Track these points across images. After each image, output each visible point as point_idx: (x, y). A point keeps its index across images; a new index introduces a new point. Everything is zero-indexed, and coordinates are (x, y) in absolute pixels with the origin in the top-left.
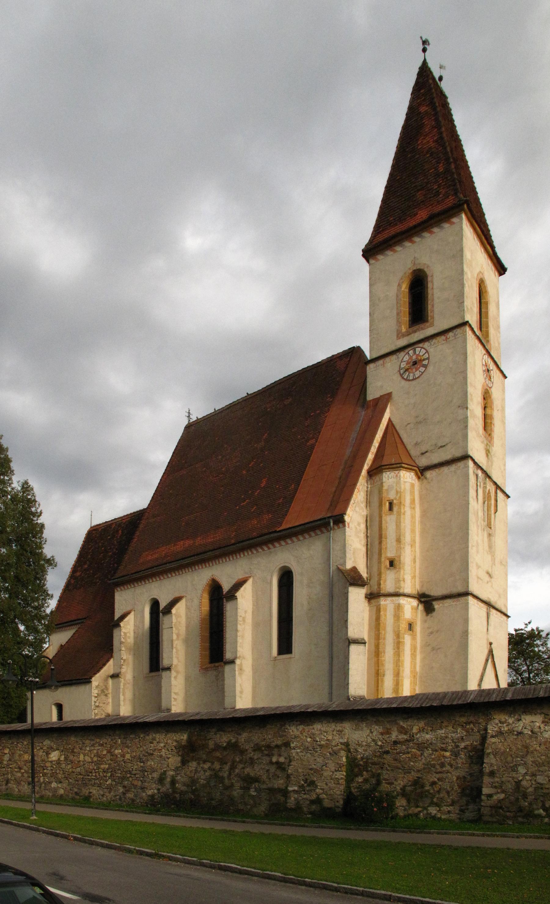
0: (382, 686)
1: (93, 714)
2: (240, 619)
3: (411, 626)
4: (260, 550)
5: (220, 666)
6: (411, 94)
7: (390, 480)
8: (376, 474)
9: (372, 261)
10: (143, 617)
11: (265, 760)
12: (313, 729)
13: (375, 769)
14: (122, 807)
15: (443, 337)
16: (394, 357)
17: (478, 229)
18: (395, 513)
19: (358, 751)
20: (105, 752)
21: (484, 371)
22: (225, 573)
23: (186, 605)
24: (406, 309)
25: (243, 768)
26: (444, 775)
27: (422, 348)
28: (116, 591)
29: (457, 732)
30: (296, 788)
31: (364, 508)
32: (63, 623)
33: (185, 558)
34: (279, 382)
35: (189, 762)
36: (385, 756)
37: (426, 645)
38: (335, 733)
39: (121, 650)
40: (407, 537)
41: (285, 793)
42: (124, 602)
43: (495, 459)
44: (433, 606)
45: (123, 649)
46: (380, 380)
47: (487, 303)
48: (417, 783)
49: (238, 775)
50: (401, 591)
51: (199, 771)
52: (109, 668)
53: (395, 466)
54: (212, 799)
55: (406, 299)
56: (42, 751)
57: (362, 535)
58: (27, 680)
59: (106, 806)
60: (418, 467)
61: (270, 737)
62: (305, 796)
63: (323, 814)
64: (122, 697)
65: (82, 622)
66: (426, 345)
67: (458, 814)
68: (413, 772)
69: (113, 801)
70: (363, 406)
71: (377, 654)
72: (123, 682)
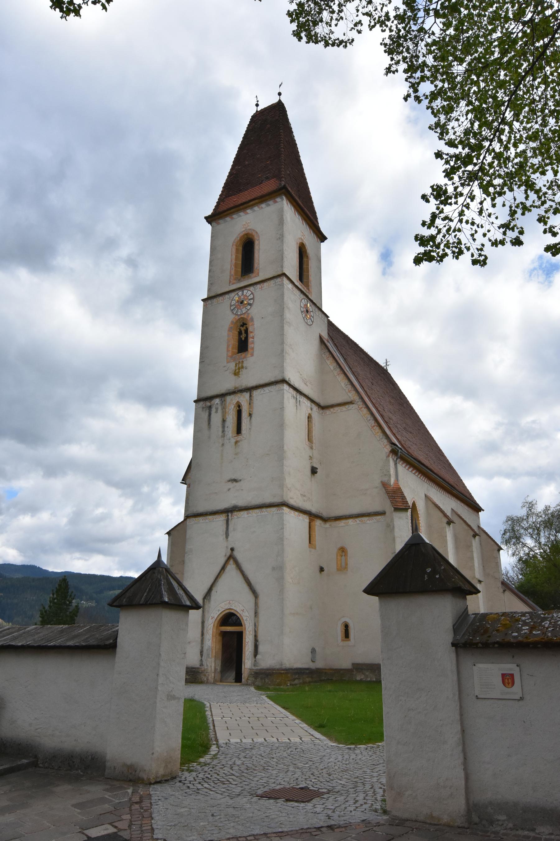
66: (252, 288)
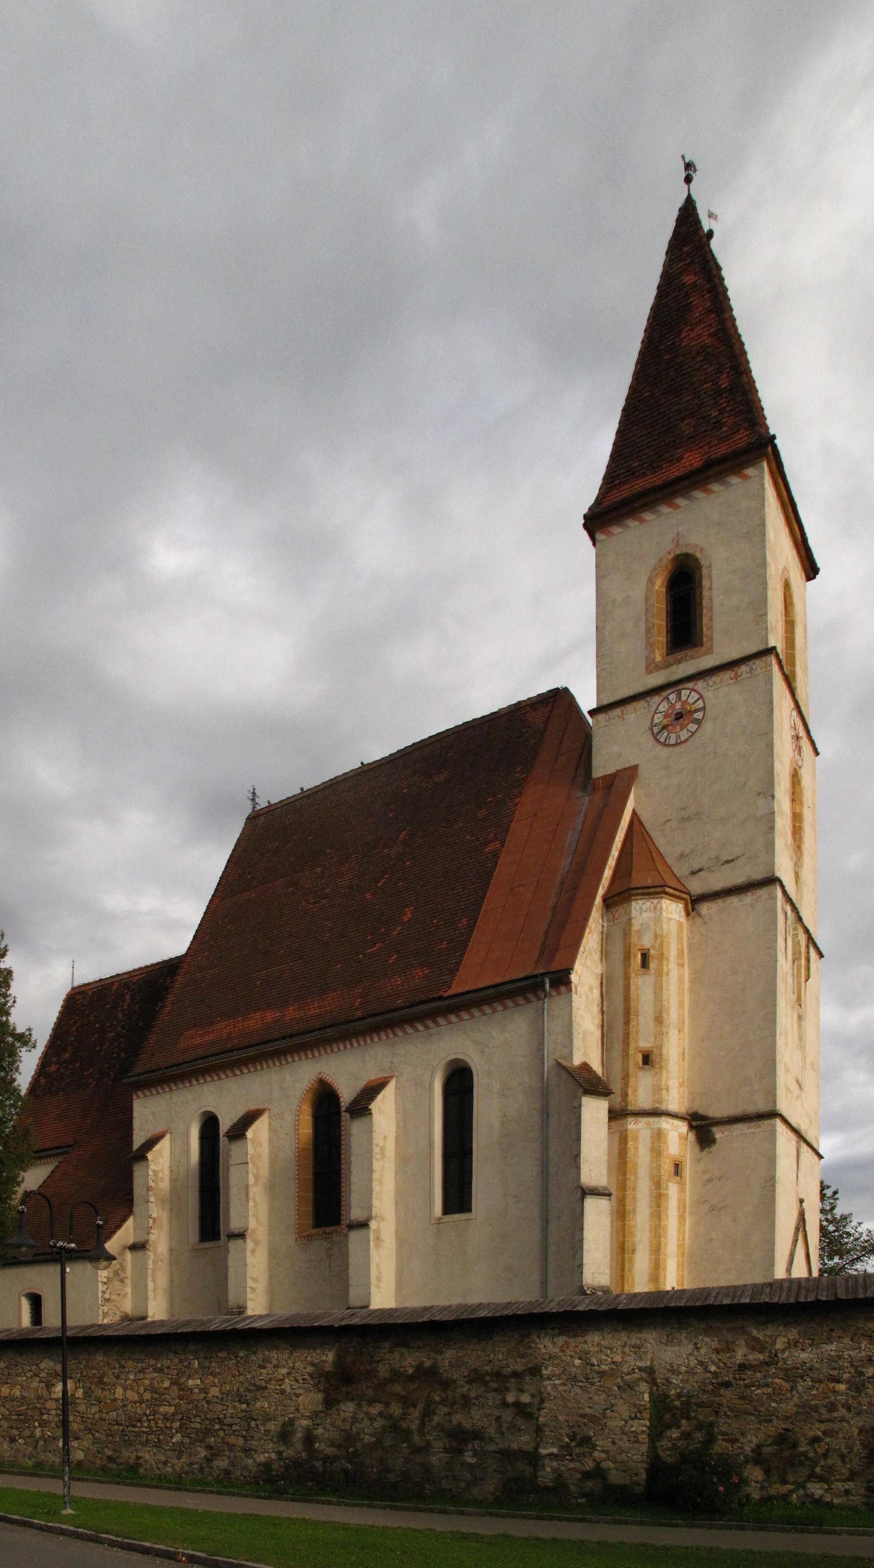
0: (630, 1270)
1: (101, 1313)
2: (376, 1150)
3: (677, 1169)
6: (667, 253)
7: (644, 915)
8: (617, 904)
9: (599, 536)
10: (188, 1145)
11: (493, 1398)
12: (586, 1342)
13: (705, 1415)
14: (207, 1484)
15: (730, 674)
16: (642, 704)
18: (652, 972)
19: (671, 1383)
20: (167, 1384)
21: (793, 736)
22: (346, 1070)
23: (270, 1124)
24: (661, 622)
25: (450, 1414)
26: (836, 1426)
28: (135, 1097)
29: (860, 1348)
30: (555, 1450)
31: (599, 961)
32: (47, 1150)
33: (267, 1042)
34: (343, 778)
35: (338, 1402)
36: (722, 1391)
37: (701, 1201)
38: (627, 1350)
39: (147, 1201)
40: (673, 1015)
41: (534, 1459)
42: (151, 1117)
43: (805, 890)
44: (713, 1136)
45: (152, 1199)
48: (783, 1439)
49: (439, 1427)
50: (663, 1107)
51: (361, 1418)
52: (126, 1233)
53: (652, 890)
54: (388, 1471)
55: (660, 606)
56: (38, 1379)
57: (596, 1009)
58: (55, 1246)
59: (177, 1483)
61: (500, 1357)
62: (572, 1465)
63: (609, 1498)
64: (151, 1285)
65: (66, 1153)
66: (700, 685)
67: (865, 1496)
68: (775, 1421)
69: (187, 1473)
70: (584, 788)
71: (621, 1216)
72: (152, 1257)
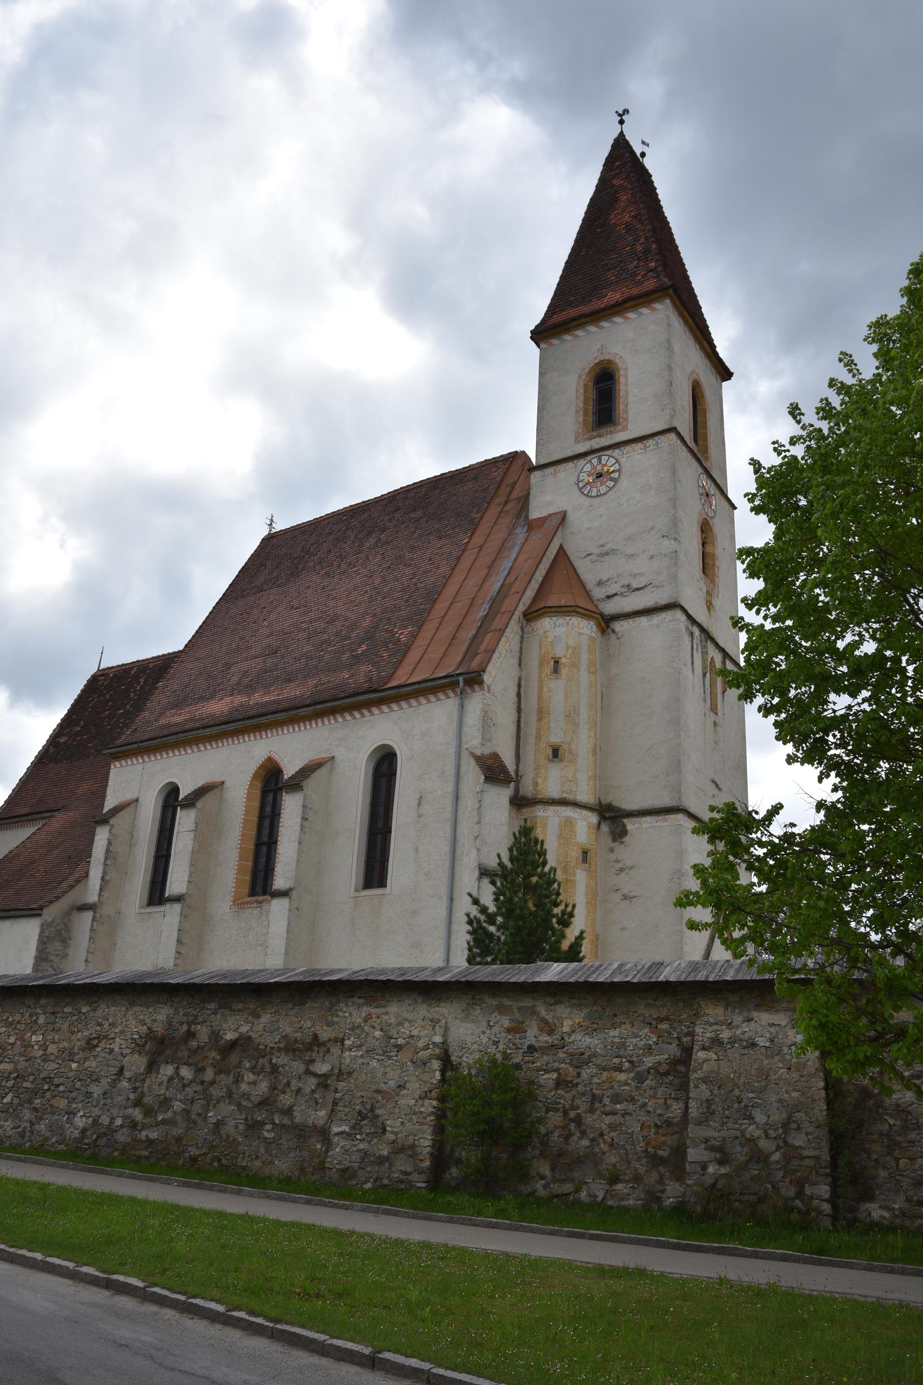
4: (349, 718)
5: (266, 901)
7: (557, 629)
9: (542, 345)
17: (690, 320)
21: (701, 494)
22: (291, 748)
27: (610, 456)
28: (112, 767)
46: (549, 496)
47: (705, 411)
53: (564, 609)
60: (601, 614)
66: (616, 453)
